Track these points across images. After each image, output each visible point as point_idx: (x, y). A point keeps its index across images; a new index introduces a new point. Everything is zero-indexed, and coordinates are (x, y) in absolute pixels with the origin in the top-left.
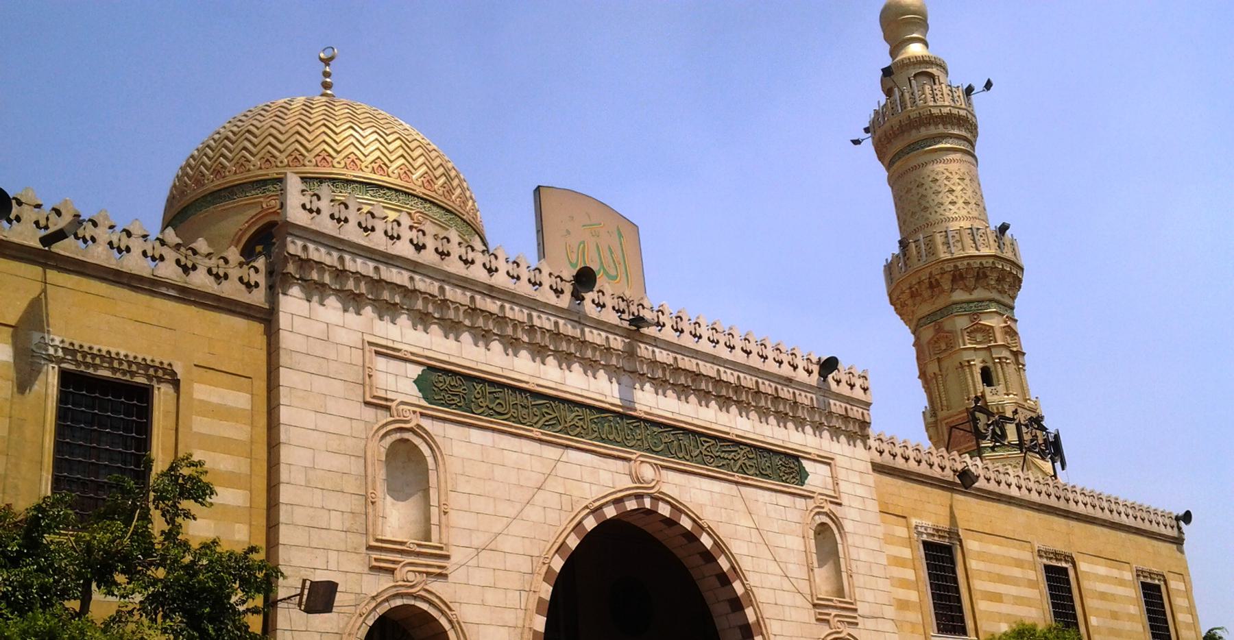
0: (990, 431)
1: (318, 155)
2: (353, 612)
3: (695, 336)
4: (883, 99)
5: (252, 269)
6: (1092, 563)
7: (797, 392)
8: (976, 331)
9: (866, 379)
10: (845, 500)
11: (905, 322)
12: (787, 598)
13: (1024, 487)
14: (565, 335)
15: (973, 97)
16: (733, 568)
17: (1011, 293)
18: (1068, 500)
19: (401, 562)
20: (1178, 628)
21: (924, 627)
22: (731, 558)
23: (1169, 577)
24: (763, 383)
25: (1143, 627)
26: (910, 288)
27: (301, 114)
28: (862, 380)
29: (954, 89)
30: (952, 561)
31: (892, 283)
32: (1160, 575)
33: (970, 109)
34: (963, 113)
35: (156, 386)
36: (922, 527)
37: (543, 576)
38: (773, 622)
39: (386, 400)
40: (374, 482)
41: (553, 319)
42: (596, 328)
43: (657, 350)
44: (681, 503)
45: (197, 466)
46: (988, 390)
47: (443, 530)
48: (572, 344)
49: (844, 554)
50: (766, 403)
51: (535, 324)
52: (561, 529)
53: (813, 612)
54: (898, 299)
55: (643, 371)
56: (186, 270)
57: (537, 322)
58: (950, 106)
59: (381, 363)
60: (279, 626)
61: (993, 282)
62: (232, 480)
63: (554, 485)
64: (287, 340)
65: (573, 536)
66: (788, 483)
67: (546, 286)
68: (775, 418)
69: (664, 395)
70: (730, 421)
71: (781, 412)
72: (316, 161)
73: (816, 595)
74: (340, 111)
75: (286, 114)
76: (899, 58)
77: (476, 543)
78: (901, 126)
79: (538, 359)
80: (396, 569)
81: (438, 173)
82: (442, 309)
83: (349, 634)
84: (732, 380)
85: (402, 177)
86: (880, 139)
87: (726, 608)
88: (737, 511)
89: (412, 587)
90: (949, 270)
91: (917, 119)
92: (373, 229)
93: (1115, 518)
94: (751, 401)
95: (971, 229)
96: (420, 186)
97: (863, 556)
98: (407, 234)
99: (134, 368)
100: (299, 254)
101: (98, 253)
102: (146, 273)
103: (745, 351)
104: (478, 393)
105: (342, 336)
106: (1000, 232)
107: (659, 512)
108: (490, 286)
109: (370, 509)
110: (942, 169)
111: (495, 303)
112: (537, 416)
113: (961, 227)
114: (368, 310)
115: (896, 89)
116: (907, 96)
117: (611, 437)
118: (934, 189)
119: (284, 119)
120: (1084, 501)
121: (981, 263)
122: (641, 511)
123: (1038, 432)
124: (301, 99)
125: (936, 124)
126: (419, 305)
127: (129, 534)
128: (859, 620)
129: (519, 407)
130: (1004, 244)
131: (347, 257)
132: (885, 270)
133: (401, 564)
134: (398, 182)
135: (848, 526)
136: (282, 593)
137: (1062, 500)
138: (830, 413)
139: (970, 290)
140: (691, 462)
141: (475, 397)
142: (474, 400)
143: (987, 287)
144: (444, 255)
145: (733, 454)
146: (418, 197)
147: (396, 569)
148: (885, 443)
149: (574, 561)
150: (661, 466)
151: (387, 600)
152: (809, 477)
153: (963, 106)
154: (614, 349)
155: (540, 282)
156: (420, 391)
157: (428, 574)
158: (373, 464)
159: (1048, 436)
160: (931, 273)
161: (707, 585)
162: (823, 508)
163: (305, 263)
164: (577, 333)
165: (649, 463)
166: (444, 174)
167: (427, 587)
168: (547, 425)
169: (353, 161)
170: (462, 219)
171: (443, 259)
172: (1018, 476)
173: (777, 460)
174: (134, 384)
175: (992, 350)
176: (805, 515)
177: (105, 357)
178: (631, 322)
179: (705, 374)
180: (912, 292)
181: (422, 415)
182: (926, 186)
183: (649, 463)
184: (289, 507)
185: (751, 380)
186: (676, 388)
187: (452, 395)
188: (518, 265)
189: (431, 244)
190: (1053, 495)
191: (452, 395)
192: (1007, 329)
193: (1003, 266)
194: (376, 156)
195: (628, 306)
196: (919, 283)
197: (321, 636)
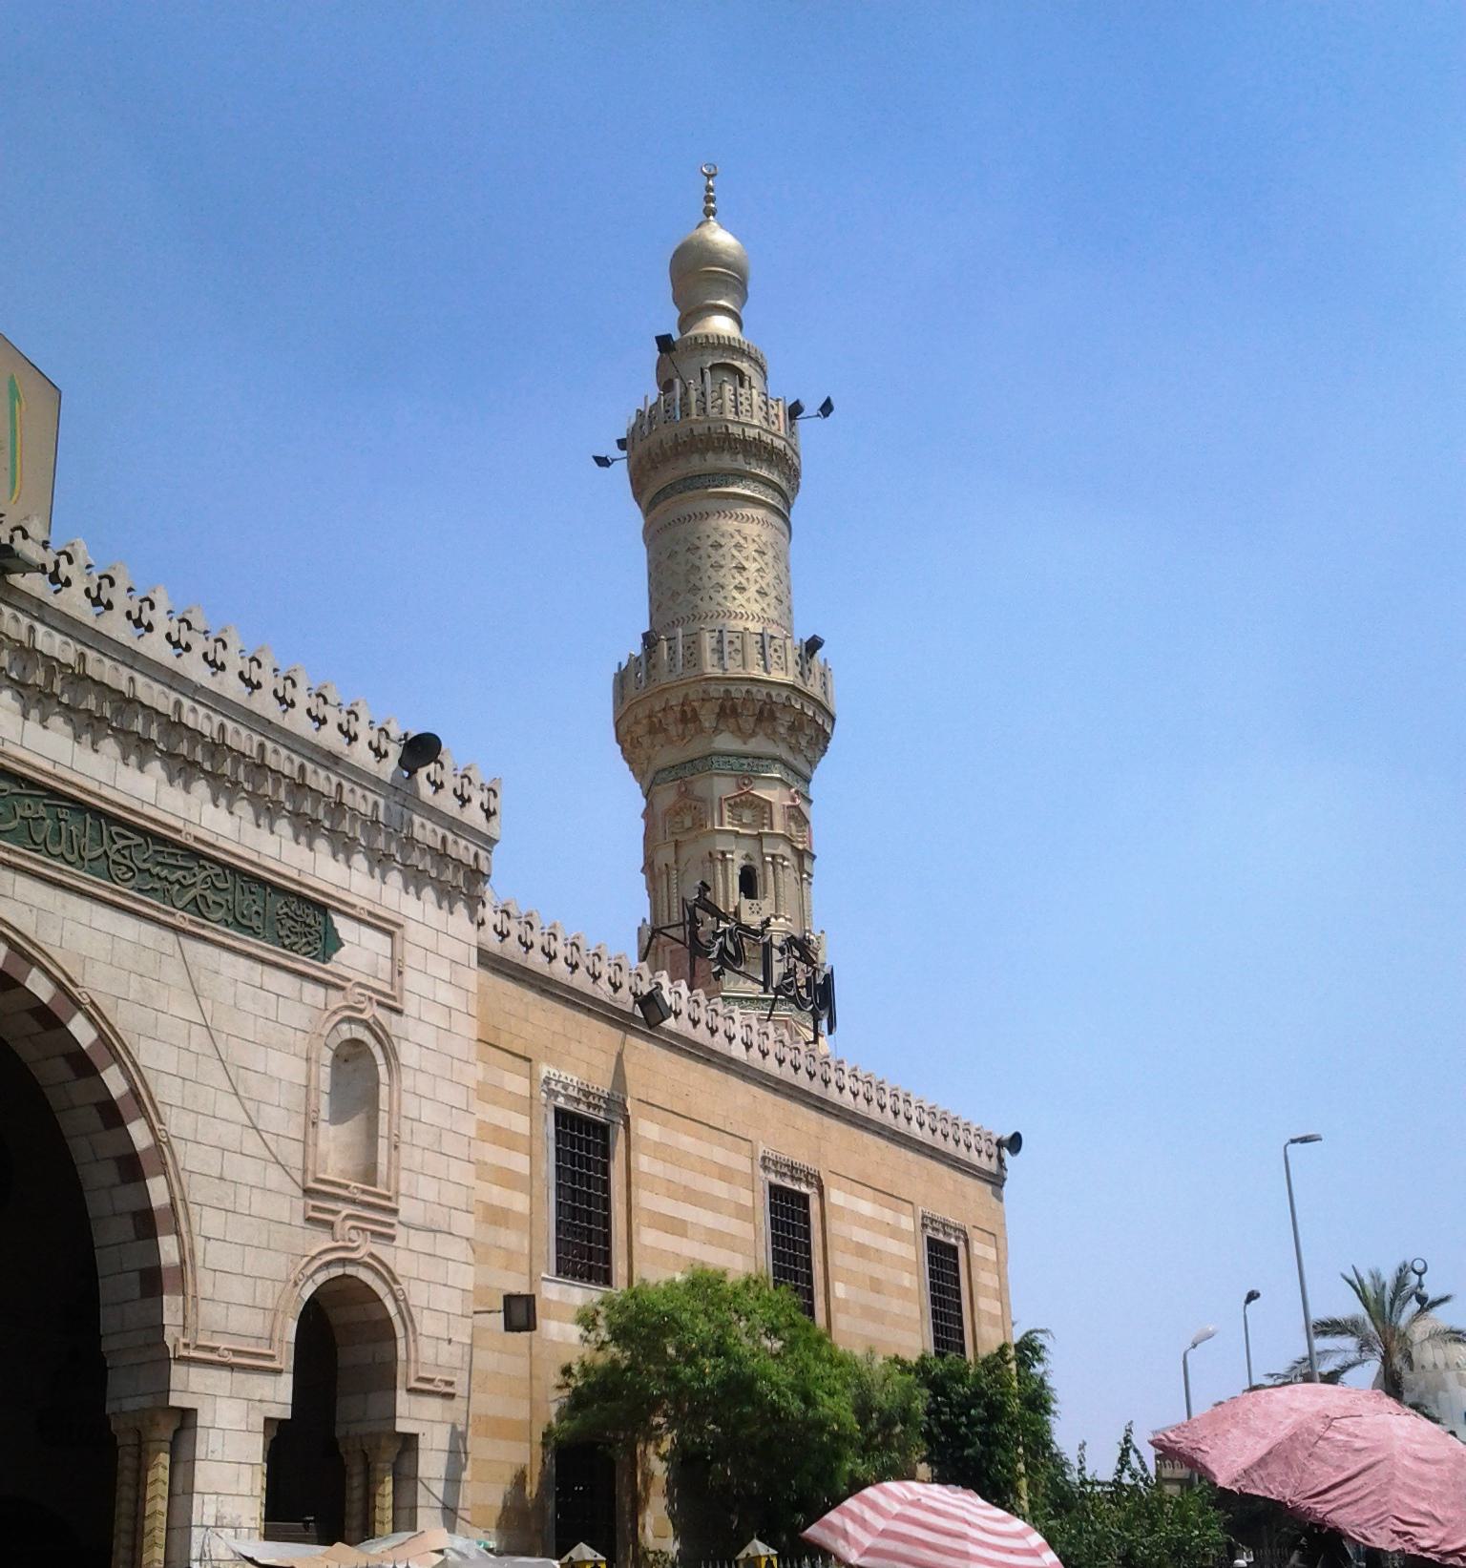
0: (717, 945)
4: (653, 393)
7: (347, 785)
8: (743, 805)
9: (495, 795)
10: (410, 1005)
12: (249, 1171)
13: (755, 1046)
16: (134, 1092)
17: (809, 755)
18: (826, 1083)
23: (975, 1236)
26: (650, 717)
29: (770, 402)
30: (606, 1152)
31: (622, 703)
32: (960, 1230)
33: (792, 441)
34: (779, 444)
36: (558, 1082)
38: (207, 1212)
43: (40, 629)
46: (746, 903)
50: (276, 791)
53: (301, 1203)
54: (629, 732)
58: (761, 428)
61: (782, 730)
66: (296, 952)
69: (43, 722)
73: (314, 1173)
76: (691, 333)
78: (676, 444)
87: (108, 1174)
90: (716, 695)
94: (242, 778)
95: (761, 635)
97: (428, 1113)
106: (807, 650)
110: (731, 529)
113: (746, 629)
115: (677, 381)
116: (693, 395)
118: (713, 560)
120: (855, 1089)
121: (769, 695)
123: (803, 966)
128: (400, 1232)
130: (810, 670)
132: (615, 681)
135: (407, 1054)
137: (817, 1080)
138: (410, 839)
139: (745, 736)
143: (773, 736)
145: (180, 873)
152: (343, 949)
153: (782, 433)
159: (814, 974)
160: (687, 695)
161: (78, 1125)
162: (361, 1011)
172: (748, 1026)
173: (278, 904)
179: (146, 703)
180: (652, 725)
182: (702, 552)
185: (250, 738)
186: (72, 716)
190: (803, 1068)
192: (793, 811)
196: (664, 710)
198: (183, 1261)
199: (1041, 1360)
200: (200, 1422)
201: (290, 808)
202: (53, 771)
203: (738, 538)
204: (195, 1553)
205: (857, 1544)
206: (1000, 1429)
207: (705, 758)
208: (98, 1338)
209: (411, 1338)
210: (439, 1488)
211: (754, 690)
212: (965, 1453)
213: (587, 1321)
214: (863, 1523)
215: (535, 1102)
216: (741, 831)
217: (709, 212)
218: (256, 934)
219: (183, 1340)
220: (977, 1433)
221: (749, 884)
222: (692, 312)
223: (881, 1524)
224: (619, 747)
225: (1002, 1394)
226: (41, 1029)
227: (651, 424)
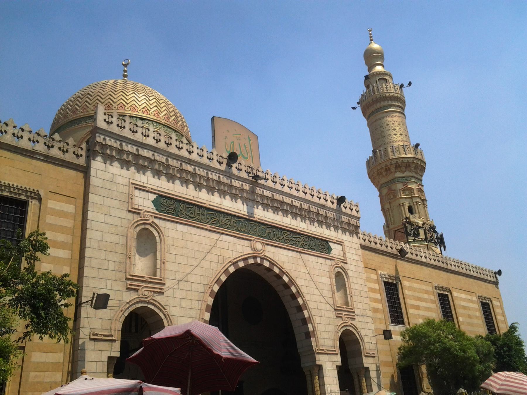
0: (413, 233)
1: (119, 105)
2: (118, 309)
3: (282, 185)
4: (365, 89)
5: (80, 148)
6: (459, 292)
8: (405, 190)
9: (358, 207)
10: (348, 261)
11: (375, 186)
12: (323, 306)
14: (223, 183)
15: (403, 89)
16: (298, 291)
18: (447, 264)
19: (141, 286)
21: (385, 320)
22: (297, 287)
23: (493, 299)
24: (312, 207)
25: (483, 322)
27: (112, 87)
28: (356, 207)
29: (395, 85)
30: (397, 290)
33: (402, 94)
34: (399, 96)
35: (30, 201)
36: (383, 274)
37: (209, 294)
39: (138, 210)
40: (130, 248)
41: (218, 175)
42: (237, 180)
43: (265, 191)
45: (42, 235)
46: (411, 216)
47: (163, 271)
48: (226, 187)
49: (349, 286)
50: (313, 216)
51: (209, 177)
52: (218, 272)
54: (372, 176)
55: (258, 200)
56: (49, 147)
57: (210, 176)
59: (137, 193)
60: (82, 315)
62: (62, 246)
63: (216, 251)
64: (94, 181)
65: (223, 275)
67: (215, 160)
68: (317, 223)
69: (267, 211)
70: (297, 224)
71: (320, 220)
72: (118, 107)
74: (130, 86)
75: (105, 87)
76: (372, 72)
77: (178, 278)
78: (373, 101)
79: (210, 193)
80: (139, 289)
81: (172, 114)
82: (167, 169)
83: (116, 320)
84: (298, 205)
85: (156, 115)
88: (300, 265)
89: (147, 298)
90: (394, 163)
91: (380, 98)
92: (136, 132)
93: (468, 272)
94: (306, 215)
95: (403, 145)
96: (164, 120)
98: (152, 135)
99: (20, 192)
100: (102, 142)
101: (7, 138)
102: (30, 148)
103: (304, 193)
104: (182, 208)
105: (119, 180)
106: (416, 147)
107: (264, 265)
108: (190, 159)
109: (128, 261)
110: (390, 120)
111: (191, 167)
112: (209, 219)
113: (399, 145)
114: (133, 169)
115: (371, 85)
116: (375, 88)
117: (243, 230)
119: (104, 89)
120: (455, 265)
122: (256, 264)
124: (113, 81)
125: (388, 100)
126: (156, 167)
127: (7, 268)
128: (356, 317)
129: (201, 215)
130: (417, 152)
131: (124, 144)
132: (366, 164)
133: (142, 287)
134: (154, 117)
135: (350, 273)
136: (84, 300)
137: (445, 264)
138: (342, 221)
139: (403, 172)
140: (279, 242)
141: (180, 210)
142: (179, 211)
143: (410, 171)
144: (169, 144)
145: (298, 239)
146: (162, 124)
147: (139, 289)
148: (366, 236)
149: (224, 287)
151: (134, 304)
153: (399, 93)
154: (245, 190)
155: (212, 158)
156: (154, 206)
157: (154, 292)
158: (131, 240)
159: (438, 235)
162: (339, 264)
163: (104, 146)
164: (228, 182)
165: (260, 242)
166: (174, 115)
167: (153, 298)
168: (213, 223)
169: (134, 108)
170: (181, 134)
171: (168, 146)
172: (425, 253)
173: (318, 242)
174: (20, 199)
176: (331, 268)
177: (7, 186)
178: (253, 177)
179: (286, 202)
181: (155, 217)
183: (260, 242)
184: (90, 259)
185: (307, 205)
187: (170, 208)
188: (203, 150)
189: (163, 139)
190: (441, 261)
191: (170, 208)
193: (417, 161)
194: (144, 106)
195: (252, 171)
196: (381, 169)
197: (102, 320)
198: (314, 329)
199: (516, 331)
201: (316, 219)
203: (393, 122)
205: (495, 388)
207: (393, 179)
208: (297, 349)
209: (363, 343)
210: (376, 380)
211: (404, 160)
213: (403, 335)
214: (495, 382)
215: (379, 281)
216: (407, 197)
217: (371, 40)
218: (314, 250)
219: (317, 348)
221: (411, 210)
222: (371, 67)
224: (370, 180)
225: (511, 343)
226: (277, 279)
227: (365, 97)
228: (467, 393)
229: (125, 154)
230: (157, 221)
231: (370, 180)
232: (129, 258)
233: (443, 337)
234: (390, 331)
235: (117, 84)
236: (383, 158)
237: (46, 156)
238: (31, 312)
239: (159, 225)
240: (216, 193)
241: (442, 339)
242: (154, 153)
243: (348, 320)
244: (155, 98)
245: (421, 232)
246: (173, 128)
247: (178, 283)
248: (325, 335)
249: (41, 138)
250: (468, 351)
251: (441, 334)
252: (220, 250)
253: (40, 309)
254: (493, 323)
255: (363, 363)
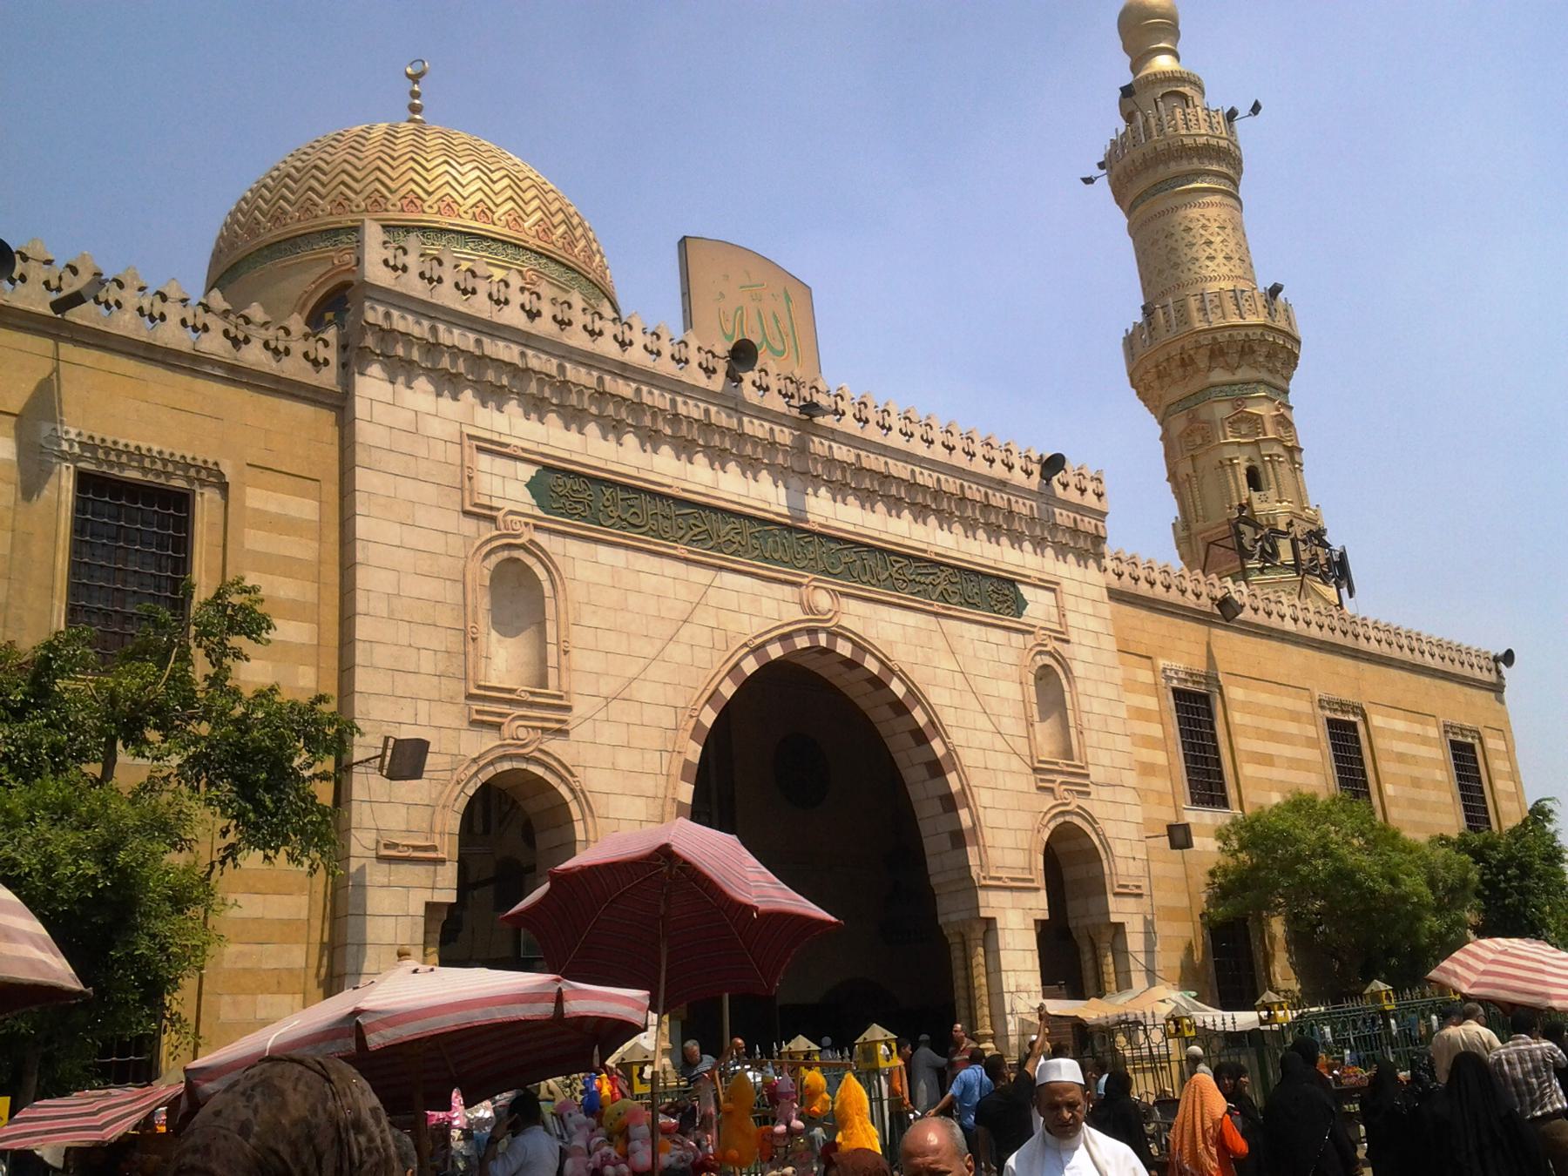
0: (1258, 549)
1: (404, 197)
3: (883, 427)
4: (1122, 126)
6: (1388, 716)
8: (1240, 420)
9: (1101, 482)
10: (1073, 636)
12: (1000, 761)
15: (1236, 123)
16: (931, 722)
18: (1356, 636)
19: (509, 714)
20: (1497, 798)
22: (928, 709)
23: (1486, 733)
24: (970, 487)
25: (1453, 797)
26: (1157, 366)
27: (383, 145)
29: (1212, 113)
30: (1210, 713)
33: (1233, 139)
34: (1223, 143)
35: (198, 491)
36: (1171, 670)
37: (690, 732)
38: (982, 791)
39: (491, 508)
40: (475, 613)
41: (702, 405)
43: (834, 445)
44: (865, 640)
45: (250, 592)
46: (1255, 495)
47: (564, 674)
49: (1073, 704)
50: (974, 512)
53: (1033, 778)
54: (1141, 380)
56: (236, 343)
57: (682, 410)
59: (484, 461)
61: (1261, 359)
62: (295, 611)
63: (705, 617)
64: (366, 432)
65: (728, 681)
67: (694, 364)
68: (985, 531)
69: (844, 502)
70: (928, 536)
74: (433, 141)
75: (363, 145)
76: (1143, 74)
78: (1145, 160)
79: (683, 457)
80: (503, 724)
81: (556, 220)
82: (561, 393)
83: (444, 807)
84: (930, 483)
86: (1118, 178)
87: (922, 772)
88: (937, 650)
89: (523, 746)
91: (1166, 152)
92: (474, 292)
93: (1417, 659)
95: (1234, 291)
96: (534, 237)
97: (1097, 707)
99: (170, 468)
102: (186, 347)
103: (947, 447)
104: (608, 500)
105: (435, 427)
106: (1271, 296)
107: (838, 651)
109: (470, 647)
111: (629, 385)
114: (468, 395)
116: (1153, 122)
117: (776, 556)
119: (361, 152)
120: (1378, 638)
121: (1247, 335)
123: (1320, 550)
124: (383, 126)
125: (1190, 158)
126: (533, 388)
127: (164, 680)
128: (1092, 788)
129: (660, 517)
130: (1276, 310)
131: (441, 327)
132: (1124, 344)
133: (510, 717)
134: (506, 231)
135: (1078, 669)
136: (358, 755)
137: (1350, 636)
138: (1055, 524)
139: (1233, 369)
141: (604, 506)
142: (602, 508)
143: (1255, 365)
144: (564, 324)
145: (931, 577)
146: (531, 251)
147: (503, 724)
148: (1125, 564)
149: (729, 713)
150: (840, 593)
151: (491, 763)
153: (1224, 135)
154: (780, 444)
156: (533, 497)
157: (544, 730)
158: (474, 590)
160: (1183, 347)
161: (899, 746)
162: (1045, 645)
163: (387, 335)
164: (734, 423)
165: (825, 589)
169: (448, 205)
171: (562, 330)
172: (1293, 605)
173: (988, 586)
175: (1261, 445)
177: (133, 453)
178: (802, 409)
179: (896, 475)
181: (536, 527)
183: (825, 589)
184: (368, 644)
185: (955, 483)
186: (859, 494)
187: (575, 502)
188: (658, 337)
189: (547, 310)
190: (1338, 629)
191: (575, 502)
192: (1279, 418)
194: (478, 199)
195: (798, 390)
196: (1168, 359)
198: (974, 824)
199: (1550, 821)
200: (999, 926)
202: (854, 530)
204: (1008, 1010)
205: (1466, 980)
206: (1531, 883)
208: (928, 877)
210: (1142, 958)
212: (1507, 902)
213: (1222, 835)
214: (1468, 967)
219: (982, 874)
220: (1514, 886)
223: (1481, 967)
225: (1530, 856)
228: (1391, 993)
229: (446, 355)
230: (542, 539)
231: (1134, 391)
232: (474, 640)
233: (1336, 843)
234: (1186, 827)
235: (397, 132)
236: (1175, 328)
237: (232, 368)
238: (238, 796)
239: (548, 550)
240: (700, 455)
241: (1333, 846)
242: (525, 350)
243: (1070, 797)
244: (507, 176)
245: (1284, 547)
246: (561, 259)
247: (606, 706)
248: (1006, 839)
249: (215, 318)
250: (1404, 880)
251: (1329, 832)
252: (717, 616)
253: (260, 787)
254: (1484, 800)
255: (1107, 913)
